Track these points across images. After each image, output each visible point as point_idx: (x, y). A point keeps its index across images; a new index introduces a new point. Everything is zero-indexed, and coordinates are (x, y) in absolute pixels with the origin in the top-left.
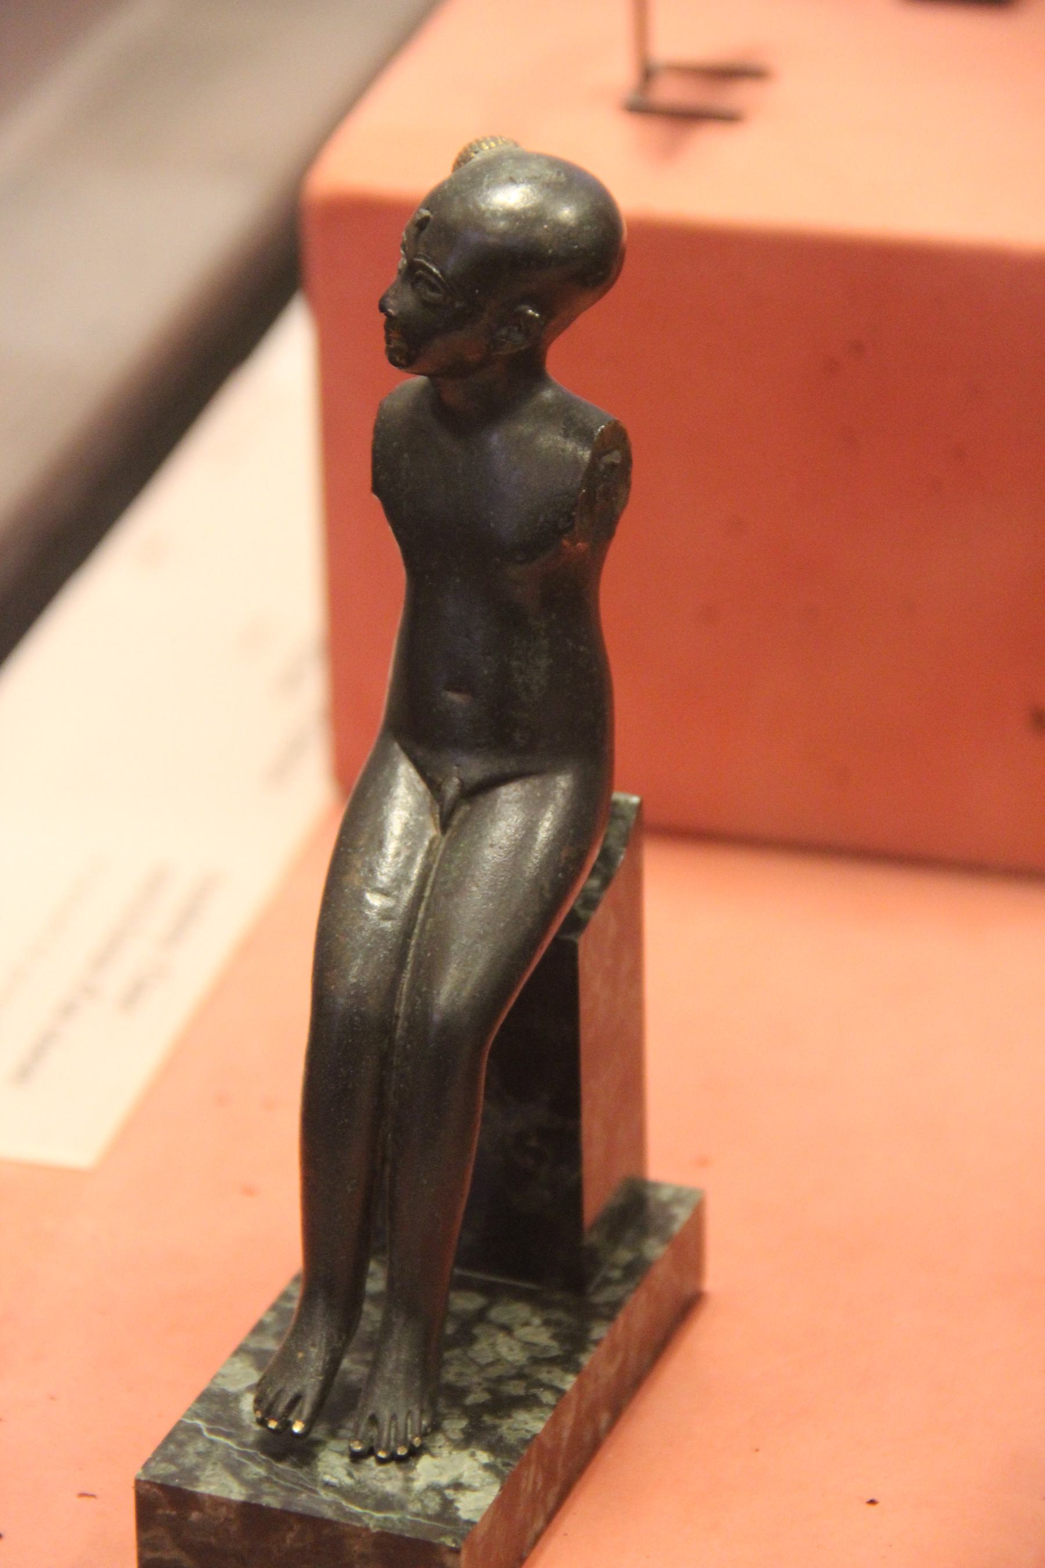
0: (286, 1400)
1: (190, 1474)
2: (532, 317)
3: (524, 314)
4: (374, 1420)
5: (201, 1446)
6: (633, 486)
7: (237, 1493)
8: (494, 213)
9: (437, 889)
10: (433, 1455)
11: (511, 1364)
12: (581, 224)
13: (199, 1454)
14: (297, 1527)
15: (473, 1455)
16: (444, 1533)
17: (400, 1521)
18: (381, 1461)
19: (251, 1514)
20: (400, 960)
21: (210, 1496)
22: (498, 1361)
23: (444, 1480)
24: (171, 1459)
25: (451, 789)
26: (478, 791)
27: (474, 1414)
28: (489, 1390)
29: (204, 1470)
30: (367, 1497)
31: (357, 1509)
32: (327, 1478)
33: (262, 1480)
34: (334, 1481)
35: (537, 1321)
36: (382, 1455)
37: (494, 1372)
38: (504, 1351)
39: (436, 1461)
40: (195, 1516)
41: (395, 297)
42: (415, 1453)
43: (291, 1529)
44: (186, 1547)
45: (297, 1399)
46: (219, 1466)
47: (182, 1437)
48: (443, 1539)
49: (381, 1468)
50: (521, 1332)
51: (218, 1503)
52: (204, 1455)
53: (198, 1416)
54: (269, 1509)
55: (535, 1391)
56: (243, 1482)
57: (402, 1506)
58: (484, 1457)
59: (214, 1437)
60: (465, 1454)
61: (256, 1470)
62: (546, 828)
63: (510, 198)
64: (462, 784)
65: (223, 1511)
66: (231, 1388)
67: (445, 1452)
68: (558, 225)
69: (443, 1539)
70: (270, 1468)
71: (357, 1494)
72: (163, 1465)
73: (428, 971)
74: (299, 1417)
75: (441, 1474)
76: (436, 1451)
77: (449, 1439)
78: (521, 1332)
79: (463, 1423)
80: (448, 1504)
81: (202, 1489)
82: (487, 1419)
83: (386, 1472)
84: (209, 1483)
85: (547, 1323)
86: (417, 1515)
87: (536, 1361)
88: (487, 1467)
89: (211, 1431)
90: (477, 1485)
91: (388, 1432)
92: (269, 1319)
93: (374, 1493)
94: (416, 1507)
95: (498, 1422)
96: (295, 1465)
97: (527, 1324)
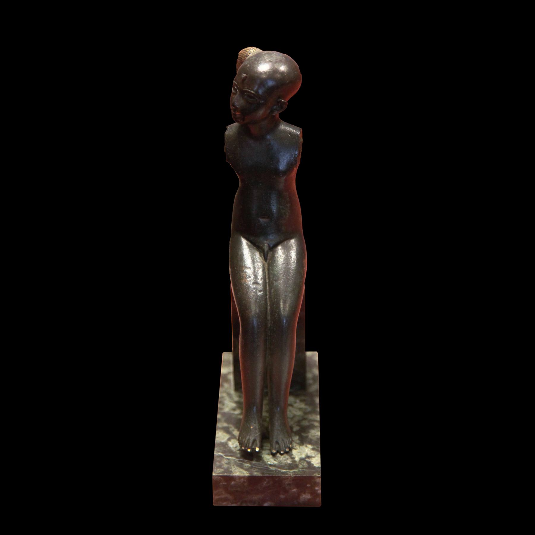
0: (251, 441)
2: (284, 102)
3: (281, 101)
4: (277, 443)
5: (226, 461)
7: (246, 474)
8: (261, 73)
9: (271, 279)
10: (295, 449)
11: (299, 416)
12: (288, 73)
13: (227, 464)
14: (267, 480)
15: (306, 446)
16: (314, 473)
17: (299, 471)
18: (282, 454)
19: (251, 479)
20: (266, 304)
21: (238, 476)
22: (295, 416)
23: (303, 456)
25: (266, 248)
26: (273, 248)
27: (298, 433)
28: (298, 425)
29: (231, 468)
30: (284, 466)
31: (284, 471)
32: (269, 463)
34: (272, 463)
35: (298, 401)
36: (282, 452)
37: (296, 419)
38: (295, 412)
39: (297, 451)
40: (233, 483)
41: (237, 102)
42: (291, 449)
43: (265, 480)
44: (230, 493)
45: (254, 441)
46: (235, 466)
48: (315, 475)
49: (282, 456)
50: (296, 405)
51: (240, 477)
52: (228, 463)
55: (311, 423)
56: (246, 470)
57: (297, 466)
58: (310, 446)
59: (228, 457)
60: (304, 447)
61: (247, 465)
62: (293, 254)
64: (269, 246)
65: (243, 479)
66: (223, 441)
67: (298, 447)
68: (282, 73)
69: (315, 475)
70: (251, 464)
71: (281, 466)
72: (218, 470)
73: (275, 305)
74: (256, 446)
75: (301, 454)
76: (295, 447)
77: (296, 443)
78: (296, 405)
79: (297, 437)
80: (309, 463)
81: (235, 474)
82: (303, 434)
83: (285, 457)
84: (236, 472)
86: (302, 468)
87: (306, 413)
88: (313, 449)
89: (226, 456)
90: (314, 455)
91: (282, 445)
93: (286, 464)
94: (301, 466)
95: (307, 435)
96: (257, 461)
97: (295, 402)
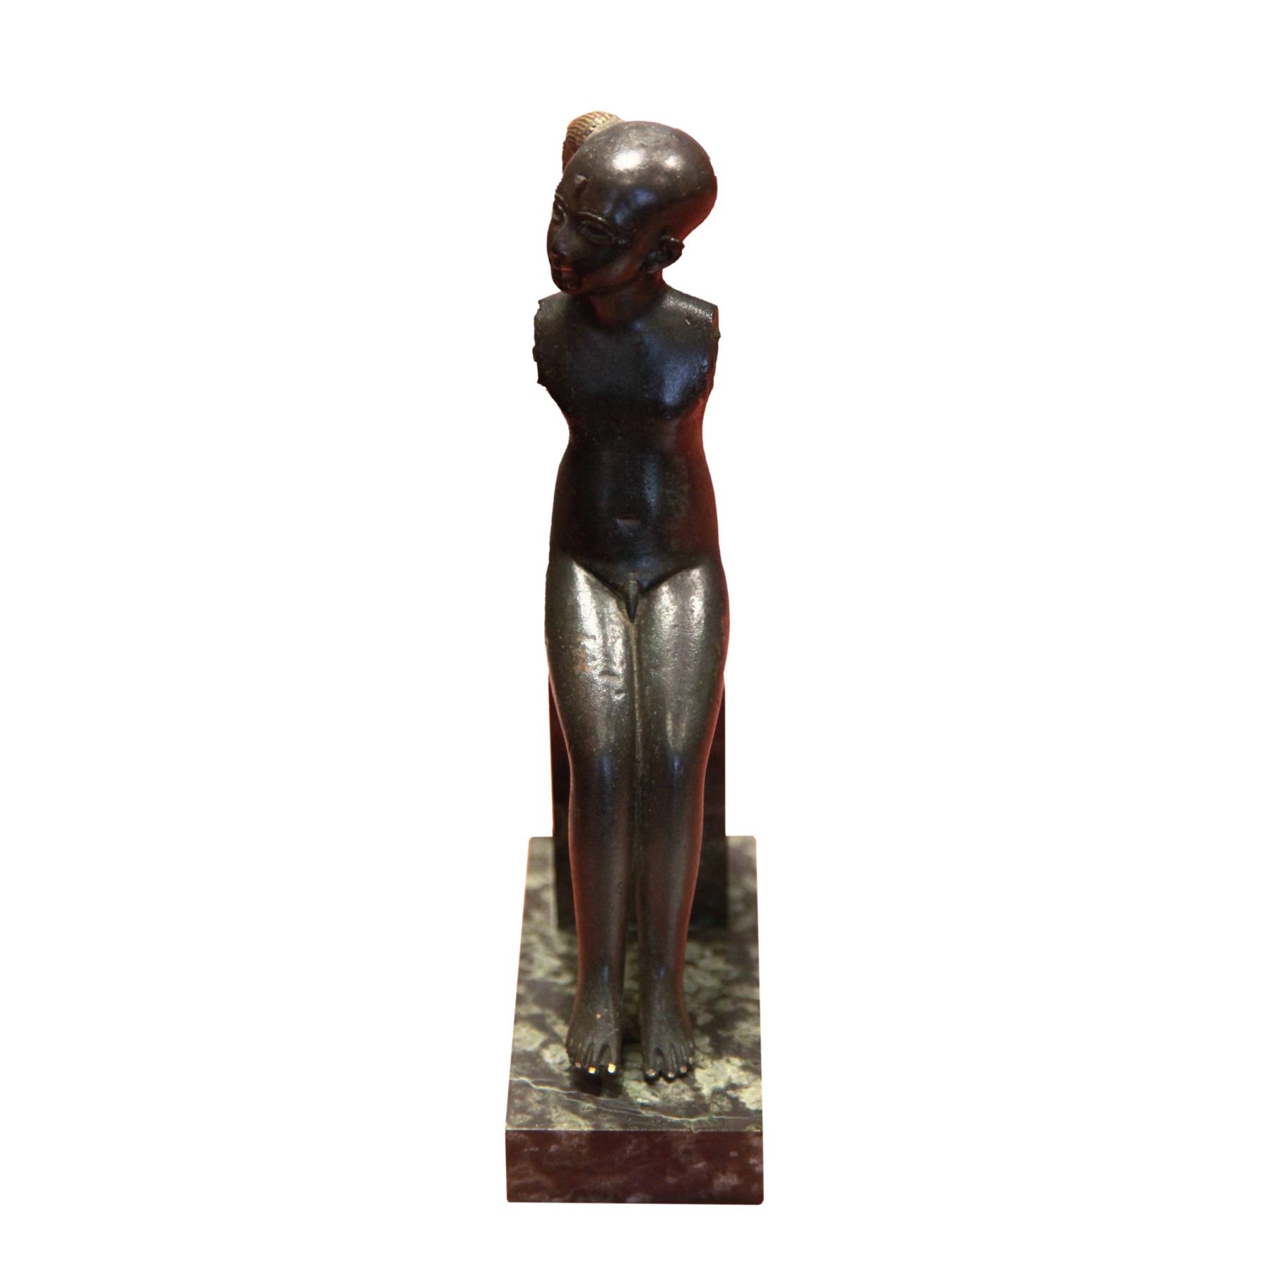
0: (597, 1048)
1: (541, 1118)
4: (659, 1052)
5: (537, 1096)
6: (532, 321)
7: (585, 1126)
8: (620, 174)
10: (702, 1068)
11: (711, 989)
13: (539, 1102)
14: (635, 1141)
15: (728, 1061)
16: (747, 1124)
17: (711, 1120)
18: (670, 1080)
19: (598, 1140)
20: (633, 722)
21: (566, 1132)
22: (700, 989)
23: (721, 1084)
24: (523, 1110)
25: (632, 589)
26: (649, 590)
27: (708, 1030)
28: (708, 1011)
29: (550, 1113)
30: (676, 1109)
31: (676, 1119)
32: (640, 1100)
33: (598, 1112)
34: (646, 1101)
35: (708, 953)
36: (670, 1075)
37: (704, 997)
38: (701, 981)
39: (706, 1071)
40: (553, 1148)
41: (565, 242)
42: (691, 1068)
43: (630, 1142)
45: (605, 1048)
46: (559, 1109)
47: (519, 1092)
48: (748, 1128)
49: (672, 1085)
50: (703, 963)
51: (570, 1135)
52: (543, 1102)
53: (520, 1074)
54: (607, 1133)
55: (739, 1005)
56: (585, 1117)
57: (705, 1109)
58: (737, 1061)
59: (541, 1088)
60: (723, 1062)
61: (588, 1106)
63: (627, 161)
64: (639, 584)
65: (577, 1140)
66: (530, 1048)
67: (708, 1062)
68: (671, 174)
69: (748, 1128)
70: (596, 1103)
71: (669, 1108)
72: (519, 1116)
73: (654, 725)
74: (610, 1061)
75: (716, 1080)
76: (702, 1064)
77: (704, 1053)
78: (703, 963)
79: (707, 1040)
80: (735, 1101)
81: (558, 1128)
82: (721, 1033)
83: (677, 1087)
84: (561, 1123)
85: (717, 953)
86: (719, 1114)
87: (727, 982)
89: (537, 1083)
90: (745, 1083)
91: (671, 1059)
92: (523, 990)
93: (680, 1104)
94: (715, 1108)
95: (729, 1033)
96: (611, 1096)
97: (703, 957)
